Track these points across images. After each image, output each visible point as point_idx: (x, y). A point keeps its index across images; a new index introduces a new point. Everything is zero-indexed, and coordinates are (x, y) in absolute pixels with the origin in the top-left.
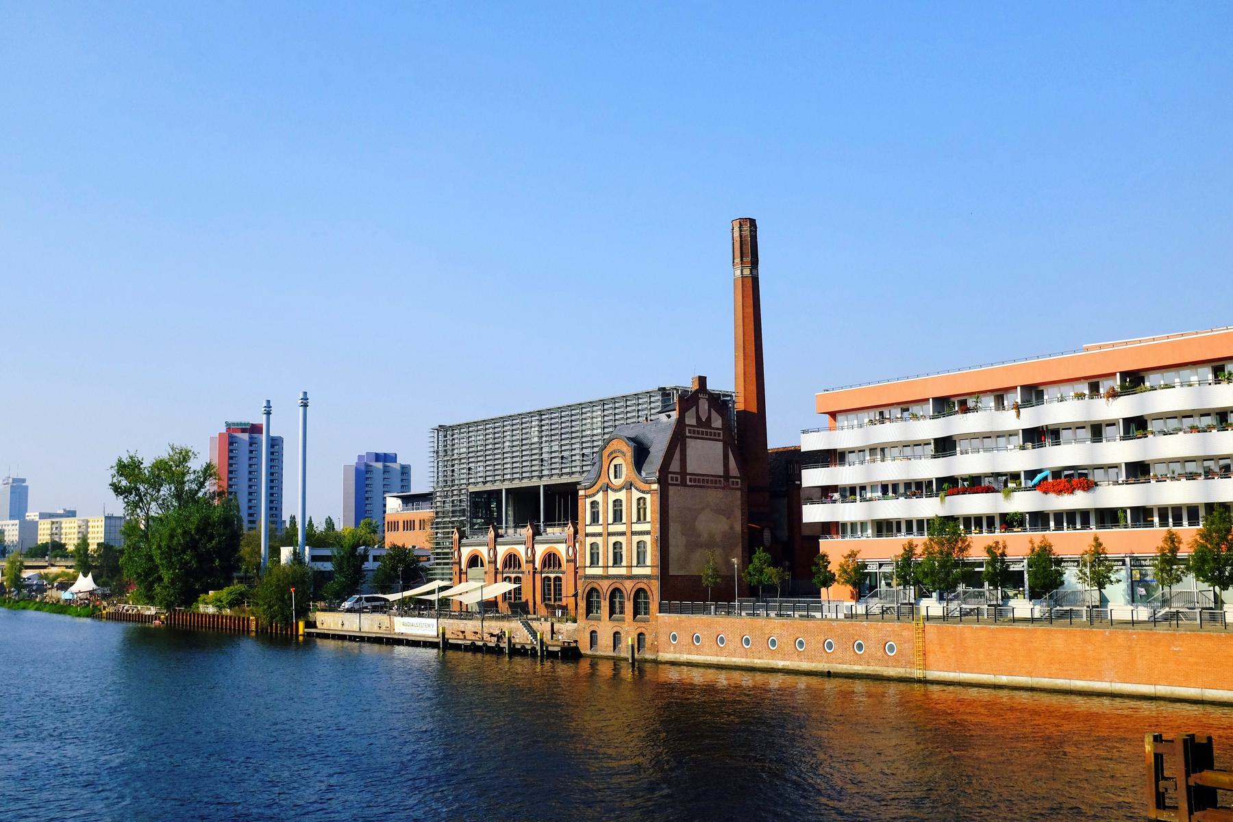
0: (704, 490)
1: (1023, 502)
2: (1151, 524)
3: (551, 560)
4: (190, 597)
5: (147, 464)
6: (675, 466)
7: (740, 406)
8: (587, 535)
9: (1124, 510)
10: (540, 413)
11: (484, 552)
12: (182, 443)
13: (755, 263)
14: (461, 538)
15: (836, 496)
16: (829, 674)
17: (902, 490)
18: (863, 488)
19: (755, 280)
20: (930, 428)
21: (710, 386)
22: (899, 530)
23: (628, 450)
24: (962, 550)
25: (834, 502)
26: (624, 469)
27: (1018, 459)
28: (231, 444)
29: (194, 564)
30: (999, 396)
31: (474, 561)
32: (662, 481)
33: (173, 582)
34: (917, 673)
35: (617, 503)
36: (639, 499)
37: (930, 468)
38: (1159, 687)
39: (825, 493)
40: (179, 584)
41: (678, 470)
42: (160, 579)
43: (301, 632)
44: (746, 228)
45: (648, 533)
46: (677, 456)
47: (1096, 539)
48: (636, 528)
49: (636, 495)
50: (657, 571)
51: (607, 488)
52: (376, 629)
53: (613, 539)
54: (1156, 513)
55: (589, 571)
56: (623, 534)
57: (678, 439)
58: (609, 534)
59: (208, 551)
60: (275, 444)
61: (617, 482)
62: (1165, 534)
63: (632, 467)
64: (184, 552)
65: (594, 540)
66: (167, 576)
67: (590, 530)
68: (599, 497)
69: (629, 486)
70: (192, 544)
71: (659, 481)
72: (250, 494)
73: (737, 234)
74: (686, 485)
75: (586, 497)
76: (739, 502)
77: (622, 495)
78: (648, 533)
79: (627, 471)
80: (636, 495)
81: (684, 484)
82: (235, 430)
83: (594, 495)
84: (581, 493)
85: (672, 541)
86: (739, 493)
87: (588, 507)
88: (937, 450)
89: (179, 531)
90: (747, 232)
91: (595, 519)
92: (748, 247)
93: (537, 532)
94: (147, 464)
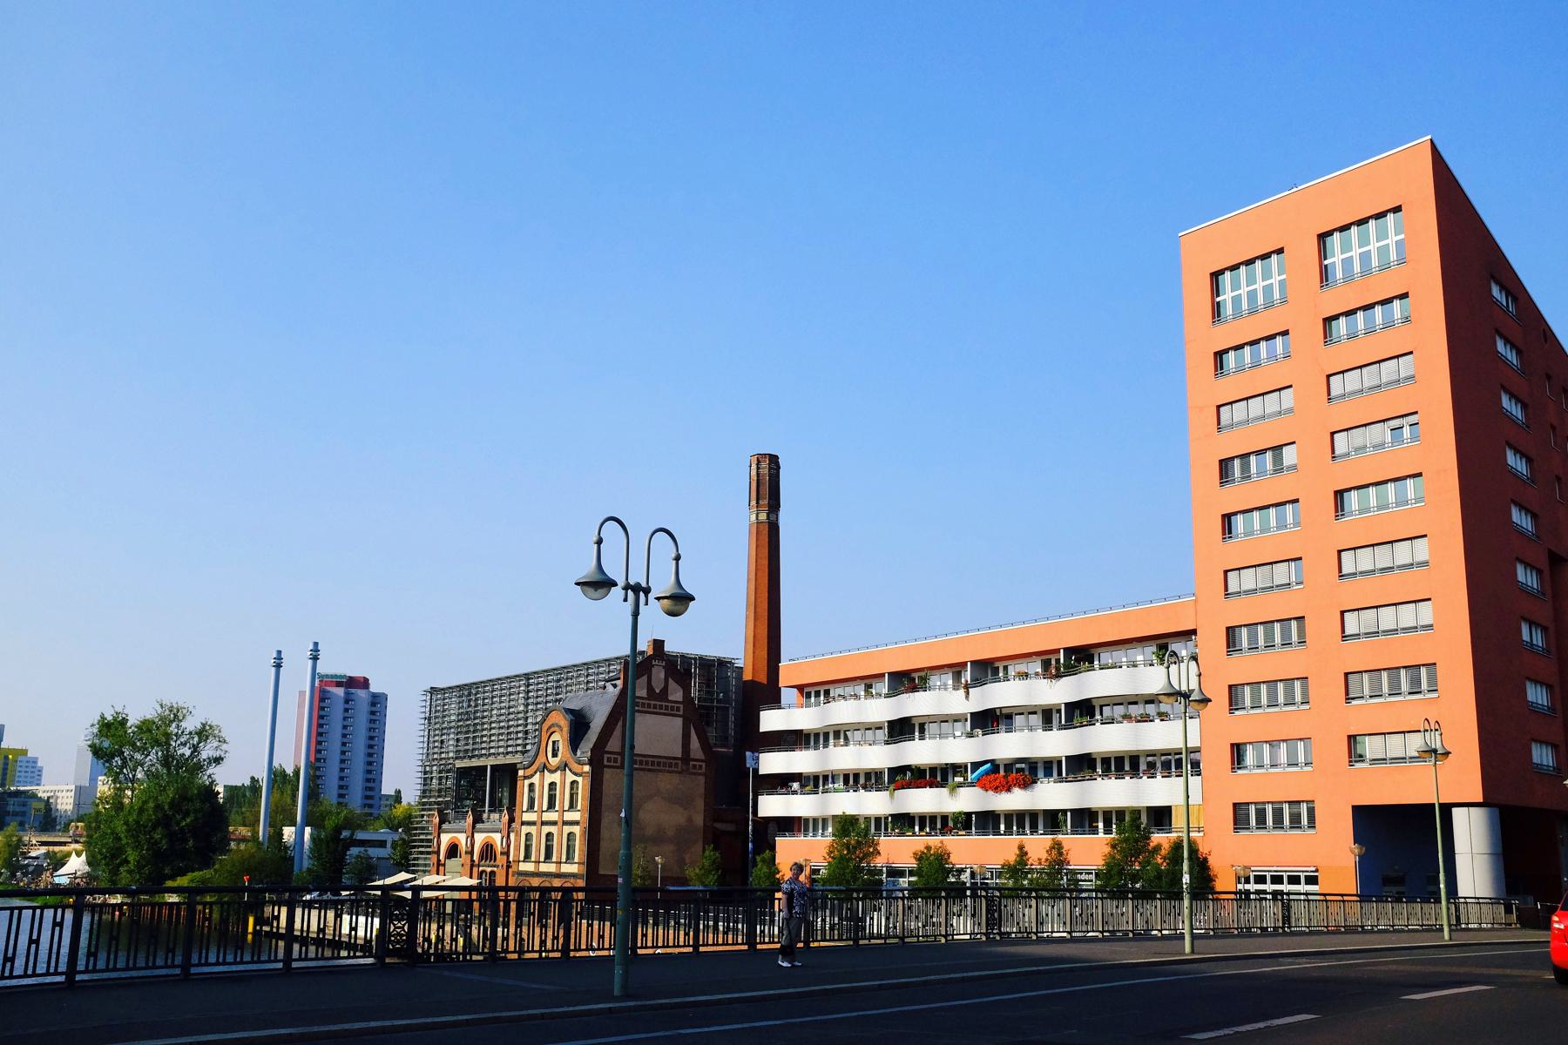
0: (650, 775)
1: (968, 800)
2: (1095, 831)
3: (488, 851)
4: (156, 885)
5: (133, 720)
6: (614, 744)
7: (747, 676)
8: (523, 823)
9: (1064, 812)
10: (527, 676)
11: (462, 839)
12: (172, 699)
13: (774, 505)
14: (442, 822)
15: (796, 786)
17: (862, 781)
18: (826, 778)
19: (773, 529)
20: (882, 709)
21: (667, 648)
22: (806, 830)
23: (563, 722)
24: (867, 855)
25: (795, 793)
27: (959, 749)
28: (322, 700)
29: (164, 845)
30: (868, 681)
31: (453, 851)
32: (596, 761)
33: (139, 866)
37: (880, 756)
39: (781, 783)
40: (146, 870)
41: (618, 749)
42: (127, 862)
43: (250, 929)
44: (765, 464)
45: (577, 823)
46: (617, 732)
47: (1021, 848)
48: (548, 816)
49: (570, 777)
50: (583, 869)
51: (544, 768)
53: (546, 829)
54: (1101, 818)
55: (524, 867)
56: (554, 823)
57: (618, 713)
58: (543, 823)
59: (182, 829)
60: (378, 701)
61: (554, 762)
62: (1048, 844)
63: (567, 743)
64: (154, 828)
66: (132, 856)
67: (527, 817)
68: (536, 779)
69: (564, 767)
70: (164, 821)
71: (591, 763)
72: (342, 761)
73: (754, 472)
75: (525, 778)
76: (702, 790)
77: (556, 777)
78: (577, 823)
79: (563, 748)
80: (570, 777)
82: (328, 683)
84: (521, 773)
85: (605, 833)
86: (702, 779)
87: (526, 789)
88: (891, 735)
89: (151, 805)
90: (765, 471)
92: (768, 486)
93: (478, 819)
94: (133, 720)
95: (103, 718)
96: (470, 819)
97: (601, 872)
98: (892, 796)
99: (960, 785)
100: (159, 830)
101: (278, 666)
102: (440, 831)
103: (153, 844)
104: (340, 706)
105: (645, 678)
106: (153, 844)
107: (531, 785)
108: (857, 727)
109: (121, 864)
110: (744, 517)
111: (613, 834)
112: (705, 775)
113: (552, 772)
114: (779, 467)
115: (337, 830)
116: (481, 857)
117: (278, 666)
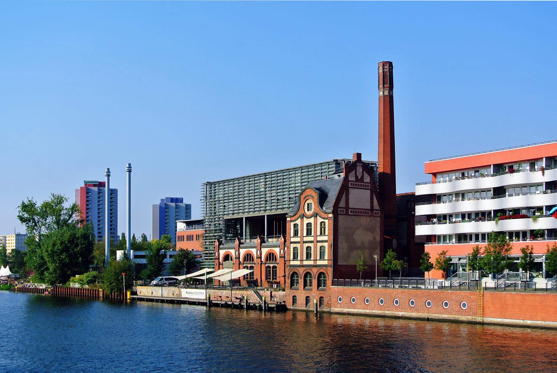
0: (357, 218)
4: (65, 279)
5: (39, 204)
6: (342, 204)
7: (381, 170)
8: (291, 243)
10: (265, 174)
11: (233, 252)
13: (391, 88)
16: (428, 319)
19: (391, 97)
20: (490, 182)
21: (364, 159)
22: (471, 239)
23: (316, 195)
25: (434, 223)
26: (313, 206)
28: (87, 193)
31: (227, 257)
33: (55, 270)
34: (479, 319)
35: (309, 225)
36: (321, 223)
37: (489, 204)
38: (374, 311)
39: (429, 219)
42: (48, 269)
43: (128, 297)
44: (387, 67)
45: (326, 241)
46: (344, 198)
49: (320, 220)
50: (331, 263)
51: (303, 216)
52: (171, 295)
53: (306, 245)
57: (345, 188)
59: (75, 253)
60: (113, 193)
65: (295, 245)
66: (51, 267)
67: (293, 240)
68: (298, 222)
69: (315, 215)
70: (66, 249)
72: (99, 221)
73: (381, 71)
74: (348, 215)
75: (291, 221)
76: (379, 224)
77: (312, 220)
78: (326, 241)
80: (320, 220)
83: (295, 220)
84: (288, 219)
85: (340, 245)
86: (379, 219)
87: (292, 227)
88: (494, 194)
89: (59, 242)
90: (387, 70)
92: (387, 79)
93: (263, 241)
95: (23, 203)
97: (339, 264)
98: (497, 223)
99: (539, 217)
100: (64, 254)
101: (130, 171)
102: (219, 249)
103: (61, 261)
105: (354, 172)
106: (61, 261)
108: (469, 191)
110: (376, 94)
111: (343, 246)
112: (380, 217)
116: (245, 260)
117: (130, 171)
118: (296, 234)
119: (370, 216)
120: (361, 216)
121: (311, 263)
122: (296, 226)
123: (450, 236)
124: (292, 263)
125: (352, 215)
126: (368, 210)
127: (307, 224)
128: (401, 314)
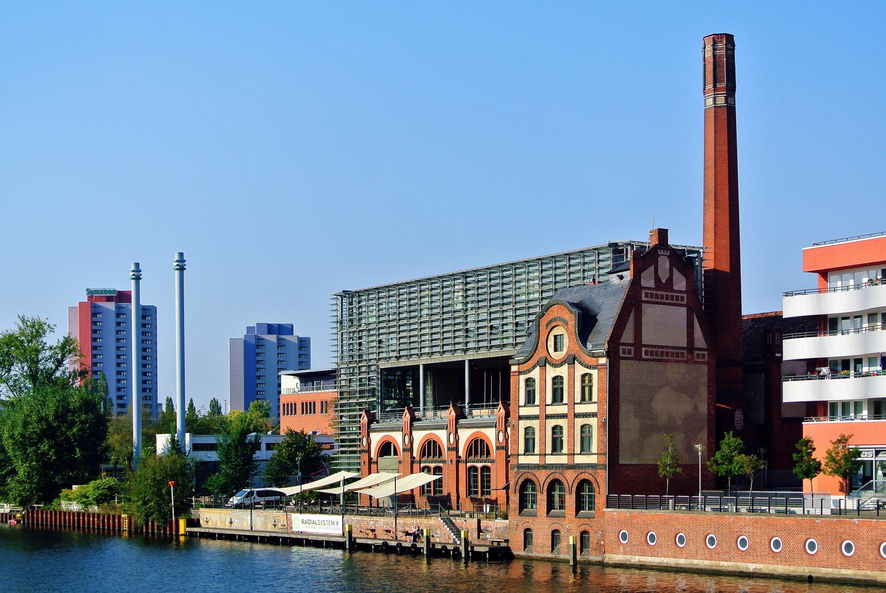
0: (660, 366)
4: (50, 492)
6: (628, 336)
7: (709, 264)
8: (520, 418)
10: (465, 275)
11: (398, 438)
13: (731, 90)
14: (370, 422)
15: (825, 370)
16: (810, 579)
19: (731, 111)
21: (672, 241)
23: (571, 318)
25: (823, 377)
26: (566, 340)
28: (94, 315)
31: (386, 449)
32: (612, 354)
33: (29, 476)
35: (557, 380)
36: (583, 376)
38: (695, 562)
39: (811, 368)
41: (631, 341)
43: (182, 530)
44: (721, 45)
45: (594, 415)
46: (630, 324)
49: (580, 370)
50: (605, 460)
51: (544, 363)
53: (551, 423)
57: (633, 304)
60: (147, 314)
64: (40, 440)
65: (529, 423)
67: (523, 411)
68: (535, 374)
69: (571, 360)
70: (49, 433)
71: (608, 354)
73: (709, 54)
75: (520, 373)
76: (705, 379)
77: (563, 371)
78: (594, 415)
80: (580, 370)
81: (638, 357)
82: (100, 299)
83: (529, 371)
84: (514, 368)
85: (623, 424)
86: (705, 368)
87: (522, 385)
89: (34, 418)
91: (530, 399)
92: (723, 71)
93: (461, 415)
96: (407, 416)
97: (621, 462)
102: (369, 430)
104: (113, 320)
105: (652, 268)
107: (529, 382)
109: (7, 475)
110: (700, 102)
111: (629, 424)
112: (708, 363)
113: (555, 365)
114: (734, 46)
115: (244, 433)
116: (423, 453)
118: (530, 399)
119: (686, 362)
120: (668, 361)
121: (563, 460)
122: (529, 382)
123: (858, 405)
124: (523, 460)
125: (647, 360)
126: (683, 348)
127: (554, 378)
128: (751, 567)
